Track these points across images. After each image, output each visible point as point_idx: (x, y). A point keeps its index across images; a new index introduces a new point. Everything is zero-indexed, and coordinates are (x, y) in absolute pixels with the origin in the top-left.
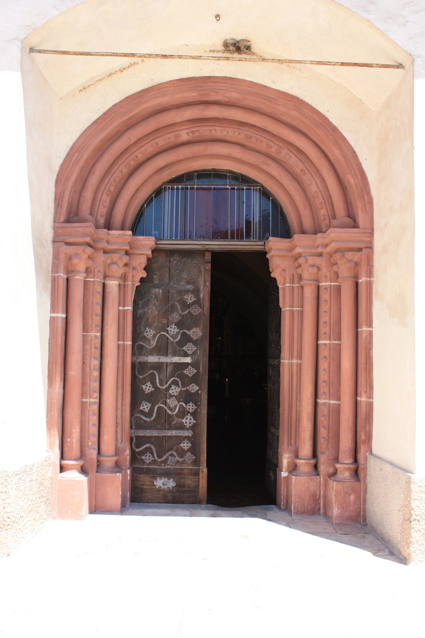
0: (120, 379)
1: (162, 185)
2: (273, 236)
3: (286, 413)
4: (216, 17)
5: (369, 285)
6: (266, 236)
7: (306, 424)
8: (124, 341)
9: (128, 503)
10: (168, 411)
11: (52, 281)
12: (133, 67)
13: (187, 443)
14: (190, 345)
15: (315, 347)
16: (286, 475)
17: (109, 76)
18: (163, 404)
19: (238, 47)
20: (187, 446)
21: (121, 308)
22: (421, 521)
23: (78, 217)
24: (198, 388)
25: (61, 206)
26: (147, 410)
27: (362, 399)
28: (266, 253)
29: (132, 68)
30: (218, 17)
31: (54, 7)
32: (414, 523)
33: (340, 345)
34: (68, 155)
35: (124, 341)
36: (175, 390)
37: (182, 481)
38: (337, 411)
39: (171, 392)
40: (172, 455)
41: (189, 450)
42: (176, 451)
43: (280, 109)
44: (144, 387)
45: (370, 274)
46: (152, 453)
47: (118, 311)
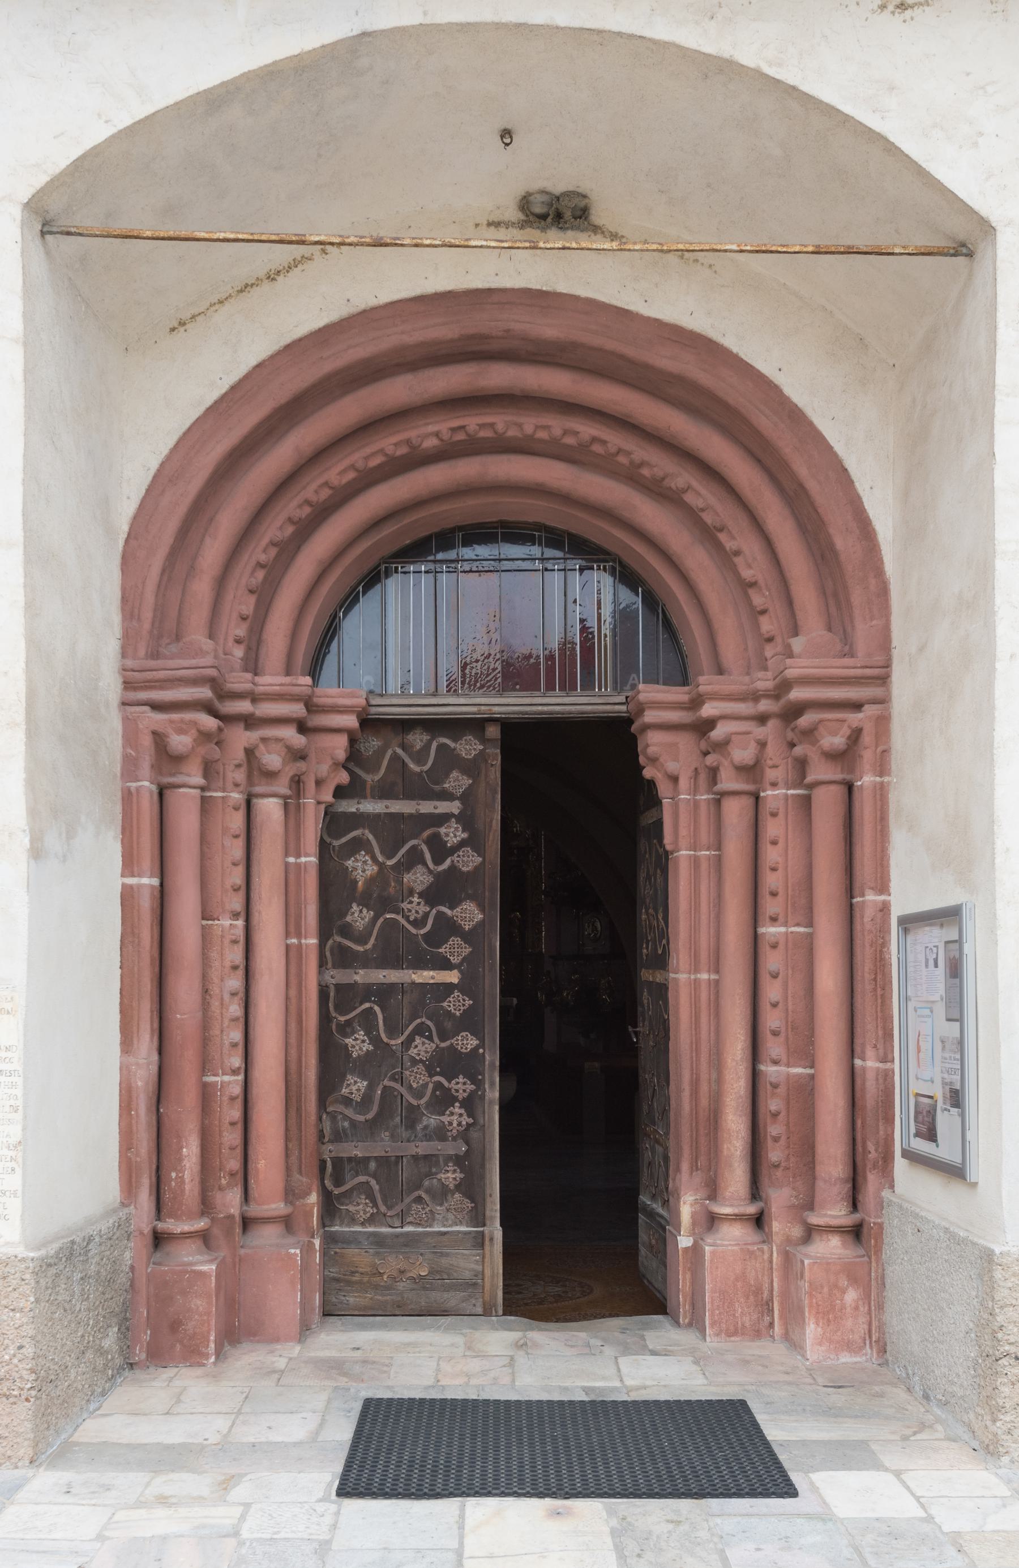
0: (293, 1026)
1: (379, 565)
3: (686, 1094)
4: (502, 137)
5: (881, 793)
6: (631, 682)
7: (735, 1124)
9: (316, 1316)
11: (123, 799)
12: (300, 267)
13: (455, 1171)
14: (455, 941)
17: (241, 291)
19: (558, 213)
20: (455, 1179)
21: (291, 860)
23: (181, 644)
25: (139, 619)
26: (357, 1097)
27: (869, 1064)
28: (629, 721)
29: (296, 271)
31: (99, 115)
32: (1007, 1364)
33: (810, 936)
34: (148, 491)
35: (299, 936)
36: (422, 1048)
37: (444, 1261)
38: (805, 1093)
39: (413, 1052)
40: (419, 1200)
41: (458, 1187)
43: (666, 359)
44: (349, 1041)
45: (882, 767)
47: (283, 868)
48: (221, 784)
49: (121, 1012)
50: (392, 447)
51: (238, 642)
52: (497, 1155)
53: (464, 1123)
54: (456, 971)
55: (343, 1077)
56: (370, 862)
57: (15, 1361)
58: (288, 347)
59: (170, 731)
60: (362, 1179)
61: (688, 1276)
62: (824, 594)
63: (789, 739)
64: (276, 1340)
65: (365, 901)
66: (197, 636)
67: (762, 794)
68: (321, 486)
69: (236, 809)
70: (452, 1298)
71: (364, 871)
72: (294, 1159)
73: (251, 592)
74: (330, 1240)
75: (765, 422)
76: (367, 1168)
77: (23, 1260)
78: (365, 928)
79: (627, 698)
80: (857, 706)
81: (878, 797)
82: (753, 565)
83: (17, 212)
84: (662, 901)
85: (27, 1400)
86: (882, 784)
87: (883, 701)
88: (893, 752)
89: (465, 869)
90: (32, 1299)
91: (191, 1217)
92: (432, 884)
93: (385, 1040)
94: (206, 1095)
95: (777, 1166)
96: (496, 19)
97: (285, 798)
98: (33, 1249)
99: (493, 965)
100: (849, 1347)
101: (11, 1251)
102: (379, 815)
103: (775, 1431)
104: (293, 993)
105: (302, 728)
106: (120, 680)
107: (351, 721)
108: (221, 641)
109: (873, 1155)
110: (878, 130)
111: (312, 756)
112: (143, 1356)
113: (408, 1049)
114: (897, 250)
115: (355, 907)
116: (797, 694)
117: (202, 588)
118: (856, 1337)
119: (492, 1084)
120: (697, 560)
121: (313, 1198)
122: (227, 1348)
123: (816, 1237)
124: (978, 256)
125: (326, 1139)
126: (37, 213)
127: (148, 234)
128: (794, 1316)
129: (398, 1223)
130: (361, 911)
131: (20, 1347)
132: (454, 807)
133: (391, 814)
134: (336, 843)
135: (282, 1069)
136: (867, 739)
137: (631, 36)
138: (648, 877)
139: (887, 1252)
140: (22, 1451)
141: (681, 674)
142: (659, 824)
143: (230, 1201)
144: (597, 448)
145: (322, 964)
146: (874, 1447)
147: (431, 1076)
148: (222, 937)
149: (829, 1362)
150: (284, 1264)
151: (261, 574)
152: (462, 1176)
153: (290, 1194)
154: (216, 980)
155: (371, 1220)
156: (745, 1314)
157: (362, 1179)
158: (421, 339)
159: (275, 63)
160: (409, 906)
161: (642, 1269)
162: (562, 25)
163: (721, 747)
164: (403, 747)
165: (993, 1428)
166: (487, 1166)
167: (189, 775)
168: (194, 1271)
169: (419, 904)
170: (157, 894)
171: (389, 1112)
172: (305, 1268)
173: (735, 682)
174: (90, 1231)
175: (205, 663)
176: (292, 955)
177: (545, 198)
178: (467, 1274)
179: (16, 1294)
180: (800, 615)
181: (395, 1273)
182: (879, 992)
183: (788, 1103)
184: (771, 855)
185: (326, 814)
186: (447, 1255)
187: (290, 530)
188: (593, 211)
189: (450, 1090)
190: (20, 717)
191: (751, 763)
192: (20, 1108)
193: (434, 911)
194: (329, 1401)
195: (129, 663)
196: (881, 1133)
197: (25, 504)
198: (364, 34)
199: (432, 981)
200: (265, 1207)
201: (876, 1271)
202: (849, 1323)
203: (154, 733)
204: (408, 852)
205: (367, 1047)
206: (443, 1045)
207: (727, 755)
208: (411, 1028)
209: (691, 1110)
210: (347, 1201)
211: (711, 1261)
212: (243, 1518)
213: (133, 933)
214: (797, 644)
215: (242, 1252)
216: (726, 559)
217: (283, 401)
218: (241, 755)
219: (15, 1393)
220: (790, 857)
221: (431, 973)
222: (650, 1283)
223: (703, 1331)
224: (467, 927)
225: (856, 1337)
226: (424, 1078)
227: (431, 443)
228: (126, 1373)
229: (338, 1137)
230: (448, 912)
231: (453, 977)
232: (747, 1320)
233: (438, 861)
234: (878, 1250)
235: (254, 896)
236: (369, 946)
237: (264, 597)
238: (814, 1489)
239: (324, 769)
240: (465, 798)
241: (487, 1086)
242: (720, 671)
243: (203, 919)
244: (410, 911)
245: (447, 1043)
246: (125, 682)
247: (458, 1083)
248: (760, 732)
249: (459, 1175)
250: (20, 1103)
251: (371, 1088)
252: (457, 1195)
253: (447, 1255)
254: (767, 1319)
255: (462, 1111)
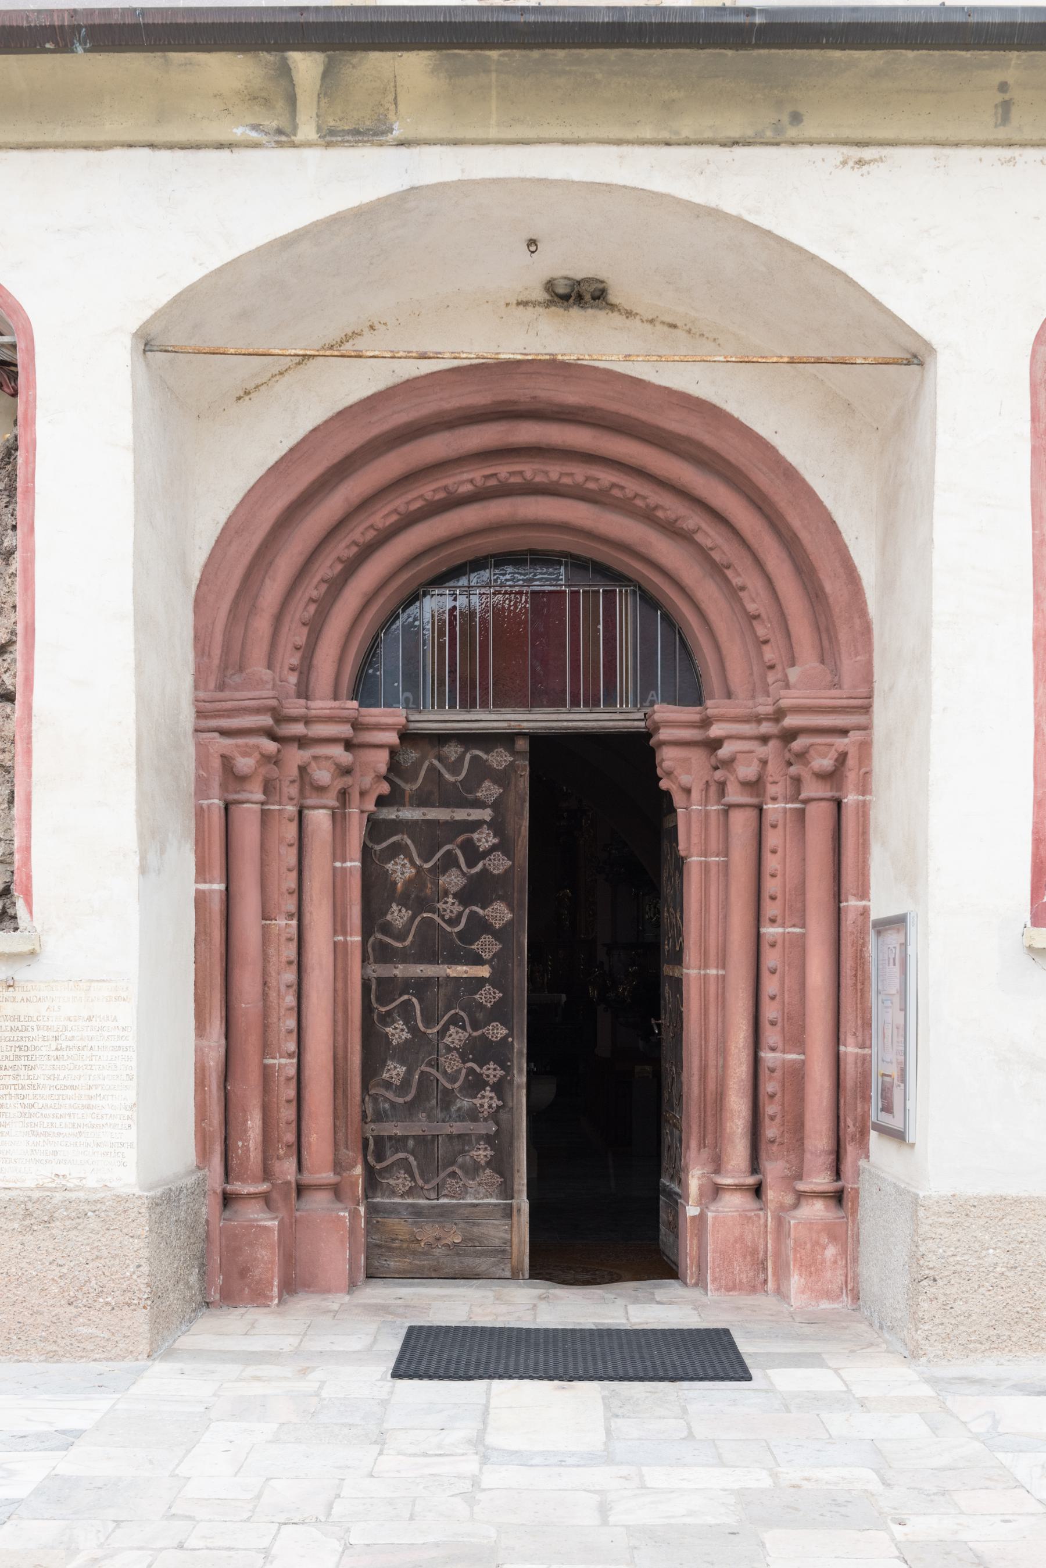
2: (664, 700)
3: (695, 1079)
4: (528, 246)
5: (863, 810)
6: (650, 698)
7: (738, 1105)
8: (345, 933)
9: (362, 1276)
10: (443, 1081)
12: (351, 342)
13: (486, 1149)
14: (487, 938)
15: (754, 938)
16: (697, 1213)
18: (432, 1066)
19: (579, 295)
20: (486, 1156)
21: (338, 864)
22: (939, 1281)
23: (244, 675)
24: (505, 1032)
25: (209, 656)
28: (648, 735)
30: (532, 242)
35: (345, 933)
36: (456, 1037)
37: (475, 1229)
38: (797, 1076)
39: (448, 1040)
40: (453, 1174)
41: (489, 1164)
42: (461, 1167)
43: (674, 422)
45: (864, 788)
46: (410, 1172)
47: (331, 873)
48: (277, 798)
49: (195, 1001)
50: (431, 493)
51: (292, 669)
52: (525, 1134)
53: (494, 1105)
54: (487, 967)
55: (384, 1063)
56: (408, 865)
57: (135, 1277)
58: (340, 413)
59: (236, 754)
60: (401, 1155)
61: (695, 1241)
62: (818, 629)
63: (787, 758)
64: (328, 1291)
65: (404, 902)
66: (258, 669)
67: (765, 807)
68: (366, 529)
69: (291, 820)
70: (483, 1264)
71: (403, 873)
72: (341, 1135)
73: (304, 624)
74: (373, 1210)
75: (763, 479)
76: (406, 1145)
77: (140, 1197)
78: (404, 926)
79: (645, 714)
80: (844, 732)
81: (861, 813)
82: (757, 601)
83: (128, 341)
84: (679, 903)
85: (144, 1307)
86: (864, 802)
87: (866, 728)
88: (873, 774)
89: (495, 872)
90: (147, 1228)
91: (255, 1181)
92: (465, 886)
93: (422, 1029)
94: (266, 1073)
95: (773, 1142)
96: (522, 175)
97: (332, 809)
98: (150, 1189)
99: (521, 961)
100: (828, 1295)
101: (129, 1191)
102: (417, 821)
103: (744, 1346)
104: (340, 985)
105: (349, 745)
106: (194, 710)
107: (392, 738)
108: (278, 669)
109: (851, 1129)
110: (838, 267)
111: (357, 769)
112: (218, 1297)
113: (443, 1038)
114: (858, 361)
115: (394, 905)
116: (791, 721)
117: (262, 624)
118: (835, 1287)
119: (520, 1070)
120: (708, 592)
121: (358, 1170)
122: (286, 1296)
123: (803, 1202)
124: (926, 366)
125: (369, 1119)
126: (141, 337)
127: (232, 351)
128: (782, 1273)
129: (433, 1195)
130: (400, 911)
131: (139, 1266)
132: (486, 814)
133: (428, 821)
134: (378, 848)
135: (330, 1054)
136: (851, 762)
137: (634, 189)
138: (669, 878)
139: (861, 1211)
140: (141, 1347)
141: (692, 692)
142: (676, 827)
143: (287, 1170)
144: (616, 492)
145: (365, 959)
146: (824, 1356)
147: (464, 1062)
148: (279, 935)
149: (811, 1308)
150: (334, 1228)
151: (312, 608)
152: (493, 1153)
153: (338, 1166)
154: (274, 974)
155: (410, 1192)
156: (742, 1271)
157: (401, 1155)
158: (458, 405)
159: (339, 213)
160: (444, 906)
161: (662, 1246)
162: (576, 178)
163: (728, 763)
164: (439, 758)
165: (916, 1337)
166: (515, 1144)
167: (251, 792)
168: (260, 1226)
169: (453, 904)
170: (224, 897)
171: (425, 1095)
172: (352, 1231)
173: (741, 705)
174: (180, 1183)
175: (265, 695)
176: (339, 951)
177: (566, 282)
178: (497, 1242)
179: (134, 1225)
180: (797, 649)
181: (431, 1240)
182: (859, 986)
183: (783, 1085)
184: (771, 863)
185: (368, 821)
186: (478, 1225)
187: (339, 567)
188: (610, 292)
189: (481, 1075)
190: (132, 759)
191: (754, 779)
192: (135, 1077)
193: (468, 757)
194: (379, 1329)
195: (202, 695)
196: (859, 1110)
197: (134, 583)
198: (412, 188)
199: (465, 975)
200: (318, 1176)
201: (852, 1230)
202: (828, 1275)
203: (223, 756)
204: (443, 855)
205: (406, 1035)
206: (475, 1034)
207: (733, 771)
208: (446, 1018)
209: (700, 1092)
210: (388, 1176)
211: (714, 1225)
212: (321, 1388)
213: (205, 932)
214: (793, 674)
215: (298, 1214)
216: (734, 593)
217: (335, 461)
218: (294, 772)
219: (136, 1302)
220: (787, 865)
221: (465, 968)
222: (668, 1257)
223: (705, 1289)
224: (497, 926)
225: (835, 1287)
226: (457, 1064)
227: (466, 488)
228: (204, 1309)
229: (380, 1117)
230: (481, 912)
231: (484, 972)
232: (744, 1276)
233: (471, 864)
234: (854, 1211)
235: (306, 897)
236: (407, 943)
237: (315, 628)
238: (767, 1377)
239: (367, 781)
240: (496, 806)
241: (515, 1072)
242: (729, 695)
243: (263, 919)
244: (445, 910)
245: (480, 1032)
246: (197, 712)
247: (488, 1069)
248: (762, 751)
249: (489, 1153)
250: (134, 1072)
251: (409, 1073)
252: (488, 1171)
253: (478, 1225)
254: (762, 1276)
255: (493, 1094)
